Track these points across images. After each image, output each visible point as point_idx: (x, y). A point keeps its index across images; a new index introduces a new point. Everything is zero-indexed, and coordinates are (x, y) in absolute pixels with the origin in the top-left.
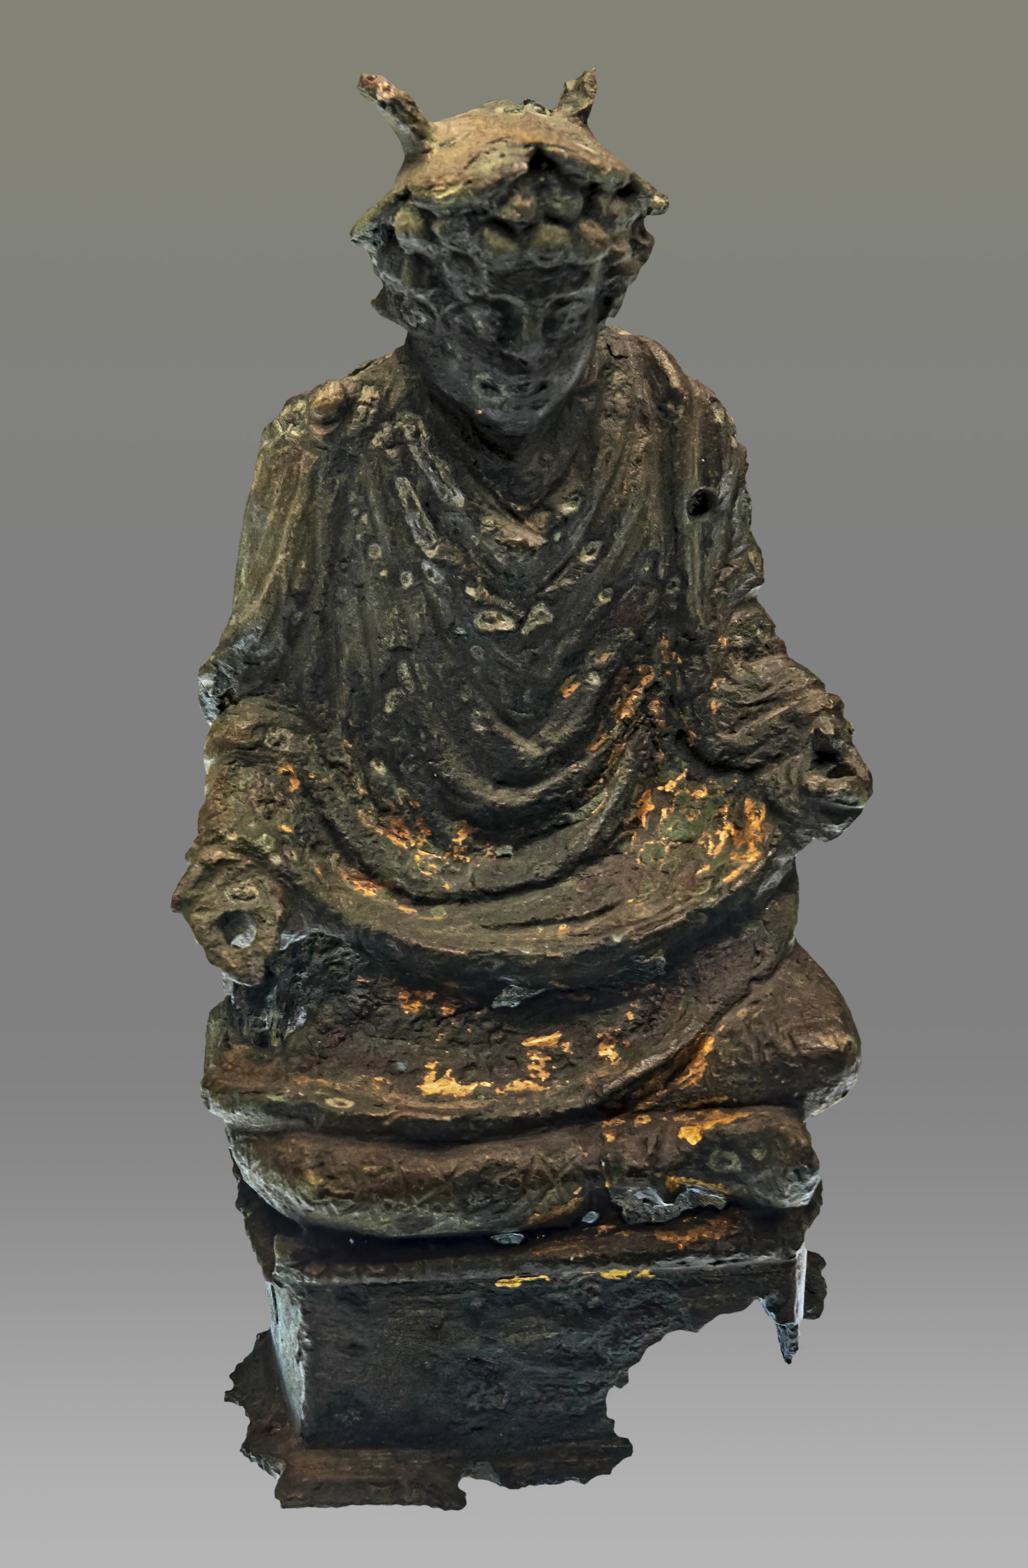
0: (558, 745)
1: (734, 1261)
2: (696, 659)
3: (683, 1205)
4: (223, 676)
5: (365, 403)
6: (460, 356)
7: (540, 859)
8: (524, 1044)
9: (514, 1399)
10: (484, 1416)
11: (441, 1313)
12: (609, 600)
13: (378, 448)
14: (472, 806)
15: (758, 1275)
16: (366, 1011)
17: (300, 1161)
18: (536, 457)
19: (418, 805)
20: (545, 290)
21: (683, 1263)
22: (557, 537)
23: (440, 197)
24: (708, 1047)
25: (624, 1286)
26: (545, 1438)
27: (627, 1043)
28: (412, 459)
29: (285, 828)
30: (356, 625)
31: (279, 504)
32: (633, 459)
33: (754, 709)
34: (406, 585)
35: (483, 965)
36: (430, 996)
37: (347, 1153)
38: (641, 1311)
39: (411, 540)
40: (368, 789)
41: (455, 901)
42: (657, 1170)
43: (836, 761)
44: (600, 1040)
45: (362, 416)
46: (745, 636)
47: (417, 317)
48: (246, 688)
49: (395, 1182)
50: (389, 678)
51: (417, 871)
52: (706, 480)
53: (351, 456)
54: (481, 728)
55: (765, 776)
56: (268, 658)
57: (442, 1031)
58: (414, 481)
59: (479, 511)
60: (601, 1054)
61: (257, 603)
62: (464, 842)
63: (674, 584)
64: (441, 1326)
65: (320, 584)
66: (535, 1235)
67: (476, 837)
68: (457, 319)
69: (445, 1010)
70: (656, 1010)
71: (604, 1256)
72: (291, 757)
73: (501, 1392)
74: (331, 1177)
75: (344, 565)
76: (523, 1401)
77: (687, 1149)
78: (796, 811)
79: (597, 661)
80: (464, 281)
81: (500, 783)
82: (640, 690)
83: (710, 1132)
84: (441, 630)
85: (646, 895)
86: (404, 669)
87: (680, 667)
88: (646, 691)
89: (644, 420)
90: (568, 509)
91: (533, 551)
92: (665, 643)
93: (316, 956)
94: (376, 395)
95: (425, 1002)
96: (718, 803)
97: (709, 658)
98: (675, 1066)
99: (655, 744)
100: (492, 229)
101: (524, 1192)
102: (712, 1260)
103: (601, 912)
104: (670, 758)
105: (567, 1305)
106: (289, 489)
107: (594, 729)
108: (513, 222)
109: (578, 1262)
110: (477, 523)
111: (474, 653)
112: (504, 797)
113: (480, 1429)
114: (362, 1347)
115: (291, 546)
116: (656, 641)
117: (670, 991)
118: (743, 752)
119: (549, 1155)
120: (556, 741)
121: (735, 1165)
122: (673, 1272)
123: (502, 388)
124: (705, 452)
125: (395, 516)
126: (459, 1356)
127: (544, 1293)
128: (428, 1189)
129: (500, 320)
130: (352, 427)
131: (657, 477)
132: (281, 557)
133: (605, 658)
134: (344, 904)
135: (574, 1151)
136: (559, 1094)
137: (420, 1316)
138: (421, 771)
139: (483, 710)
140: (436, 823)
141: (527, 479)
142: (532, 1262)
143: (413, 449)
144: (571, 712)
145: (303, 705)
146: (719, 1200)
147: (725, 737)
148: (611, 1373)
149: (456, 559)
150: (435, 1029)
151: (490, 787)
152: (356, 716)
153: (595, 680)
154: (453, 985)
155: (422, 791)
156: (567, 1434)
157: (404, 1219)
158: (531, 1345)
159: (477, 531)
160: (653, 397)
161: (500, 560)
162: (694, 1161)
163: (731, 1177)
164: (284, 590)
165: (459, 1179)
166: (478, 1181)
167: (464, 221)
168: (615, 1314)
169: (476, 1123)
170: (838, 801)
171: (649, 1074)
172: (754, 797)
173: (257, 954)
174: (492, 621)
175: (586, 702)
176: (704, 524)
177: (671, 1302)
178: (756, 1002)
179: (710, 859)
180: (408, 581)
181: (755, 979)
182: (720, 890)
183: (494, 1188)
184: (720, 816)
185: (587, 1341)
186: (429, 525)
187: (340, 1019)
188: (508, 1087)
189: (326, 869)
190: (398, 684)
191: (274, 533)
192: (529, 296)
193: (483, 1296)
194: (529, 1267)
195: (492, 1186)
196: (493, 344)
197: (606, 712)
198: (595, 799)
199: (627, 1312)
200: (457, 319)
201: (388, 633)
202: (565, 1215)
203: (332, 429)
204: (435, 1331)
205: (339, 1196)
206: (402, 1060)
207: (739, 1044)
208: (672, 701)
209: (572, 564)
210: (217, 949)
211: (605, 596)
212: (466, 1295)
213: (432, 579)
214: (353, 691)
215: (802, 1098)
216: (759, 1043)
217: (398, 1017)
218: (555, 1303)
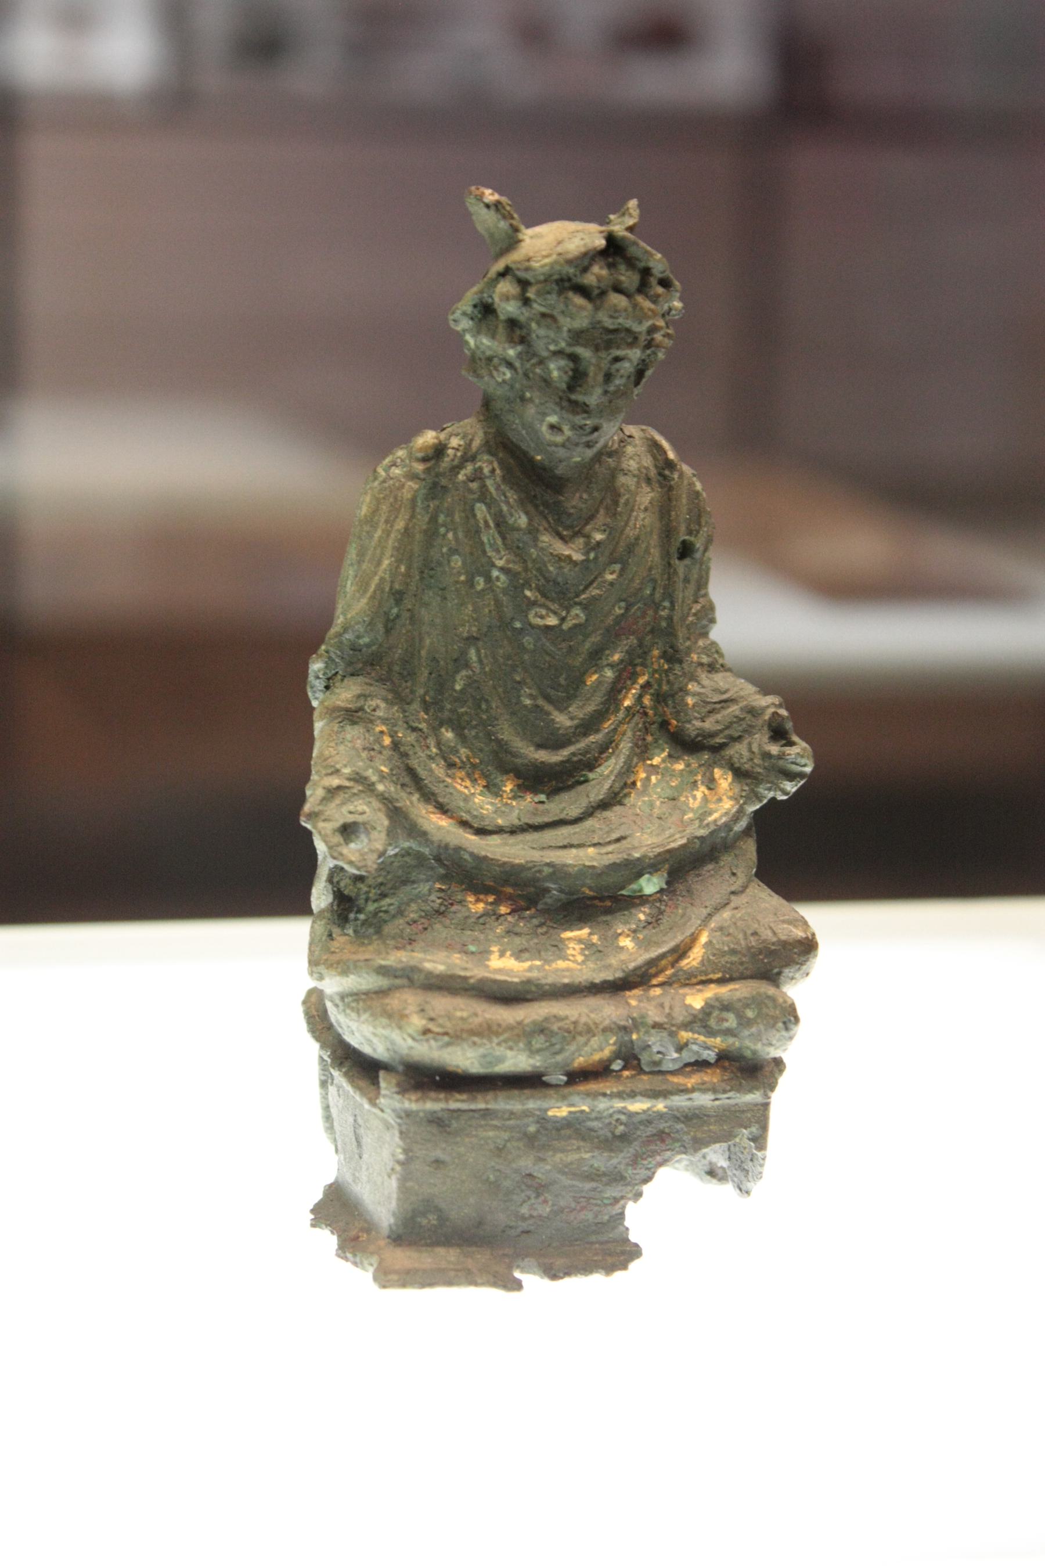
0: (582, 719)
1: (728, 1098)
2: (677, 666)
3: (687, 1057)
4: (333, 660)
5: (453, 448)
6: (537, 401)
7: (569, 804)
8: (562, 936)
9: (555, 1208)
10: (531, 1222)
11: (506, 1135)
12: (622, 611)
13: (464, 482)
14: (518, 761)
15: (743, 1112)
16: (443, 908)
17: (405, 1009)
18: (578, 495)
19: (478, 761)
20: (609, 345)
21: (690, 1099)
22: (592, 555)
23: (538, 265)
24: (704, 939)
25: (644, 1117)
26: (576, 1240)
27: (641, 936)
28: (487, 490)
29: (383, 768)
30: (438, 621)
31: (387, 522)
32: (642, 507)
33: (718, 706)
34: (479, 588)
35: (536, 872)
36: (491, 899)
37: (441, 1003)
38: (656, 1138)
39: (484, 552)
40: (440, 749)
41: (506, 832)
42: (673, 1025)
43: (786, 739)
44: (620, 934)
45: (451, 457)
46: (708, 656)
47: (504, 374)
48: (350, 669)
49: (481, 1025)
50: (460, 662)
51: (476, 810)
52: (690, 532)
53: (442, 487)
54: (528, 702)
55: (729, 752)
56: (368, 646)
57: (501, 924)
58: (489, 507)
59: (538, 530)
60: (622, 944)
61: (364, 601)
62: (511, 790)
63: (665, 608)
64: (505, 1146)
65: (413, 587)
66: (578, 1076)
67: (519, 786)
68: (538, 371)
69: (503, 910)
70: (661, 913)
71: (633, 1091)
72: (384, 721)
73: (545, 1201)
74: (432, 1019)
75: (432, 573)
76: (562, 1210)
77: (694, 1012)
78: (759, 770)
79: (611, 659)
80: (547, 337)
81: (540, 746)
82: (638, 687)
83: (710, 999)
84: (505, 624)
85: (649, 831)
86: (472, 654)
87: (666, 671)
88: (642, 687)
89: (648, 480)
90: (599, 537)
91: (575, 563)
92: (656, 653)
93: (370, 903)
94: (462, 443)
95: (486, 903)
96: (692, 773)
97: (685, 665)
98: (681, 952)
99: (646, 729)
100: (575, 293)
101: (574, 1038)
102: (713, 1097)
103: (618, 840)
104: (656, 741)
105: (601, 1132)
106: (395, 510)
107: (607, 710)
108: (591, 286)
109: (612, 1096)
110: (536, 540)
111: (526, 644)
112: (543, 756)
113: (528, 1232)
114: (443, 1162)
115: (395, 553)
116: (650, 651)
117: (670, 900)
118: (713, 735)
119: (592, 1012)
120: (581, 716)
121: (731, 1021)
122: (682, 1107)
123: (566, 428)
124: (690, 511)
125: (473, 533)
126: (517, 1171)
127: (584, 1121)
128: (505, 1031)
129: (572, 370)
130: (445, 463)
131: (658, 525)
132: (386, 562)
133: (616, 657)
134: (426, 826)
135: (608, 1010)
136: (594, 970)
137: (489, 1138)
138: (481, 735)
139: (529, 688)
140: (490, 775)
141: (572, 511)
142: (579, 1094)
143: (489, 483)
144: (593, 696)
145: (393, 682)
146: (710, 1056)
147: (698, 724)
148: (629, 1188)
149: (517, 568)
150: (496, 924)
151: (532, 749)
152: (432, 693)
153: (609, 674)
154: (509, 890)
155: (481, 750)
156: (593, 1238)
157: (484, 1056)
158: (571, 1163)
159: (536, 546)
160: (656, 467)
161: (551, 569)
162: (700, 1021)
163: (729, 1032)
164: (387, 589)
165: (527, 1025)
166: (541, 1029)
167: (554, 286)
168: (635, 1139)
169: (537, 986)
170: (793, 763)
171: (663, 956)
172: (721, 767)
173: (372, 851)
174: (542, 617)
175: (603, 688)
176: (686, 566)
177: (678, 1132)
178: (736, 908)
179: (692, 810)
180: (480, 583)
181: (733, 893)
182: (708, 825)
183: (553, 1034)
184: (696, 782)
185: (615, 1161)
186: (499, 542)
187: (423, 914)
188: (554, 965)
189: (411, 803)
190: (467, 666)
191: (381, 544)
192: (597, 349)
193: (538, 1122)
194: (576, 1099)
195: (552, 1032)
196: (564, 391)
197: (615, 700)
198: (606, 764)
199: (645, 1139)
200: (538, 371)
201: (463, 625)
202: (601, 1061)
203: (429, 465)
204: (500, 1151)
205: (438, 1034)
206: (472, 944)
207: (729, 935)
208: (660, 698)
209: (600, 579)
210: (339, 849)
211: (620, 608)
212: (526, 1120)
213: (499, 584)
214: (430, 674)
215: (779, 973)
216: (745, 934)
217: (467, 914)
218: (591, 1130)
